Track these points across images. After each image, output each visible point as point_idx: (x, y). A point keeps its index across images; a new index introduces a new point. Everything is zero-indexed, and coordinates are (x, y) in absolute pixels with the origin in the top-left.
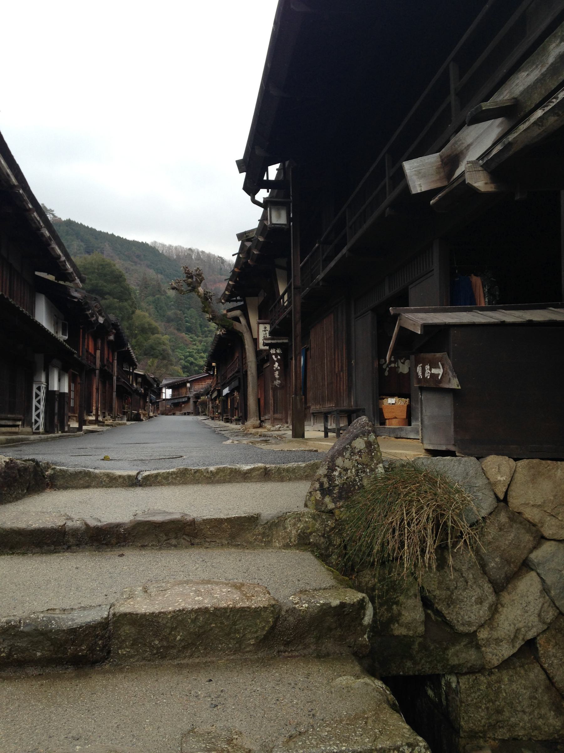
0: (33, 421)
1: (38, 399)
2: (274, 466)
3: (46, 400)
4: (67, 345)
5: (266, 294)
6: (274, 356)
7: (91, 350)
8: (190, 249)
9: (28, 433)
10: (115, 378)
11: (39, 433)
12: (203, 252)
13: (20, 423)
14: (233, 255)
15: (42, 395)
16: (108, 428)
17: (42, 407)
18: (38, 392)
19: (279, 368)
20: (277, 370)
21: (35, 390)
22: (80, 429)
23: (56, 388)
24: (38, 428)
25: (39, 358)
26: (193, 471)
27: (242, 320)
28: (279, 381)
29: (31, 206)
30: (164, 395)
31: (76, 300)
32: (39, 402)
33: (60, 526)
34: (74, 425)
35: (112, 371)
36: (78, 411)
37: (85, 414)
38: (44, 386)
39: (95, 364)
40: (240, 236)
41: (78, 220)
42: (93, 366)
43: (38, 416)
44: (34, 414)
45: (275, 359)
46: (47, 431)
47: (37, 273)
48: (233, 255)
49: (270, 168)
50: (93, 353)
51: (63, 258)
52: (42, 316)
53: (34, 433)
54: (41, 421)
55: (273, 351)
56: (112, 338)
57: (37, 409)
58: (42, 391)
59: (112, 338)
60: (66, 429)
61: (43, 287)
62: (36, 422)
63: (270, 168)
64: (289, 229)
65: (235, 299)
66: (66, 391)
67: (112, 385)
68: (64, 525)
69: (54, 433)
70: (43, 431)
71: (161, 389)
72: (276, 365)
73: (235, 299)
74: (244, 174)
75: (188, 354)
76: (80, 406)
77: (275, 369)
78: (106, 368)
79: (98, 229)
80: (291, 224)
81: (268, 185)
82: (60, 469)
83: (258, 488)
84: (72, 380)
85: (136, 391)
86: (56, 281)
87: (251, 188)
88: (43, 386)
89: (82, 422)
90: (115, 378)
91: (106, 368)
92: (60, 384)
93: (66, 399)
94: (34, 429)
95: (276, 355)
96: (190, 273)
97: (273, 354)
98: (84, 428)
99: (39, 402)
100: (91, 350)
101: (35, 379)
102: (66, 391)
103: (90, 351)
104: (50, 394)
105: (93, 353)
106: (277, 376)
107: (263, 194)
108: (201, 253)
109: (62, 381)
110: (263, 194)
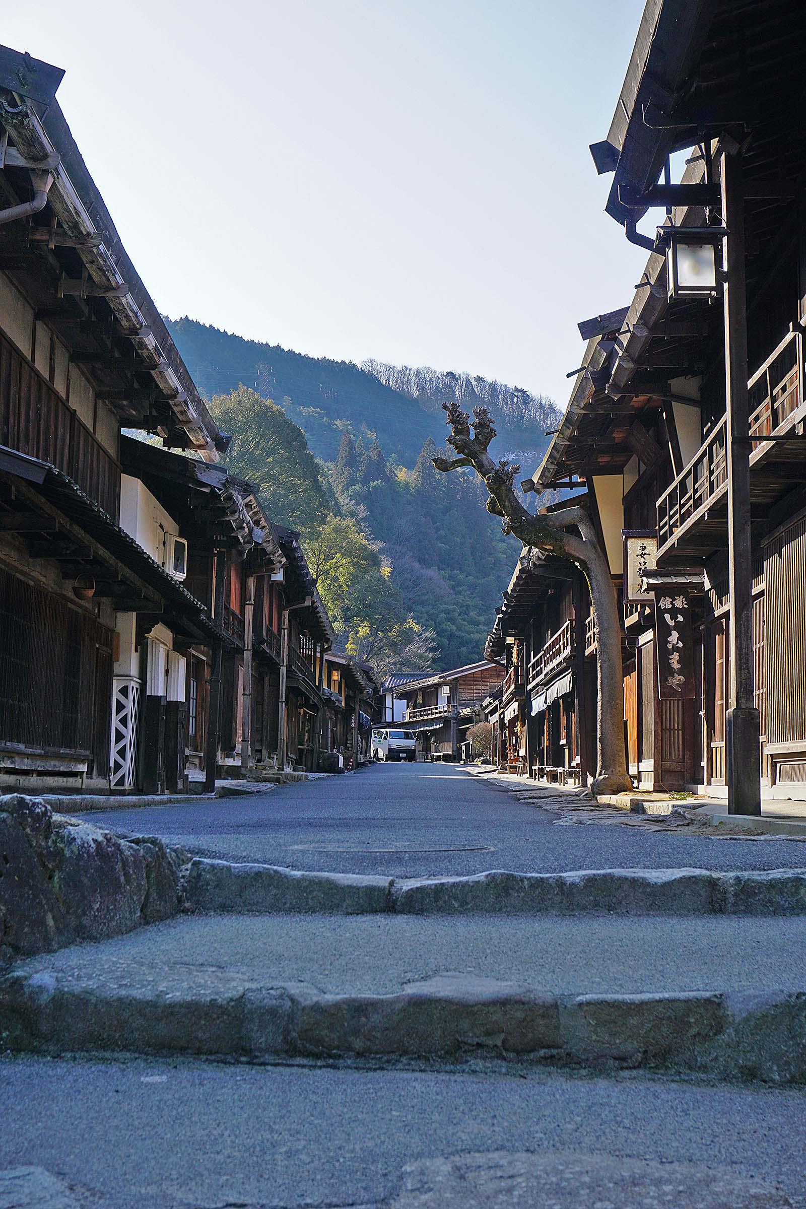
0: (112, 764)
1: (122, 715)
2: (732, 874)
3: (139, 717)
4: (186, 592)
5: (643, 467)
6: (667, 617)
7: (234, 605)
8: (451, 374)
9: (100, 792)
10: (283, 670)
11: (123, 793)
12: (479, 379)
13: (83, 768)
14: (569, 376)
15: (131, 707)
16: (269, 785)
17: (129, 734)
18: (122, 699)
19: (680, 645)
20: (675, 649)
21: (116, 695)
22: (208, 786)
23: (161, 693)
24: (121, 782)
25: (127, 625)
26: (526, 882)
27: (583, 530)
28: (682, 678)
29: (121, 281)
30: (389, 712)
31: (207, 490)
32: (124, 721)
33: (231, 1000)
34: (197, 775)
35: (278, 654)
36: (204, 745)
37: (219, 753)
38: (136, 686)
39: (241, 637)
40: (587, 329)
41: (205, 320)
42: (238, 643)
43: (122, 753)
44: (114, 749)
45: (672, 623)
46: (138, 790)
47: (125, 431)
48: (569, 376)
49: (673, 157)
50: (237, 612)
51: (182, 396)
52: (140, 517)
53: (112, 793)
54: (128, 765)
55: (666, 603)
56: (279, 577)
57: (120, 737)
58: (131, 698)
59: (279, 577)
60: (180, 786)
61: (136, 459)
62: (118, 766)
63: (673, 157)
64: (719, 301)
65: (567, 480)
66: (182, 698)
67: (276, 686)
68: (242, 997)
69: (155, 793)
70: (132, 787)
71: (381, 700)
72: (675, 635)
73: (567, 480)
74: (610, 176)
75: (443, 615)
76: (210, 733)
77: (670, 646)
78: (265, 646)
79: (246, 338)
80: (726, 286)
81: (671, 196)
82: (212, 866)
83: (700, 929)
84: (194, 671)
85: (328, 702)
86: (166, 449)
87: (625, 207)
88: (134, 684)
89: (214, 771)
90: (283, 670)
91: (265, 646)
92: (171, 682)
93: (181, 716)
94: (112, 784)
95: (674, 612)
96: (471, 421)
97: (667, 611)
98: (218, 783)
99: (124, 721)
100: (234, 605)
101: (117, 668)
102: (182, 698)
103: (232, 607)
104: (151, 707)
105: (237, 612)
106: (676, 666)
107: (653, 220)
108: (474, 383)
109: (172, 673)
110: (653, 220)
